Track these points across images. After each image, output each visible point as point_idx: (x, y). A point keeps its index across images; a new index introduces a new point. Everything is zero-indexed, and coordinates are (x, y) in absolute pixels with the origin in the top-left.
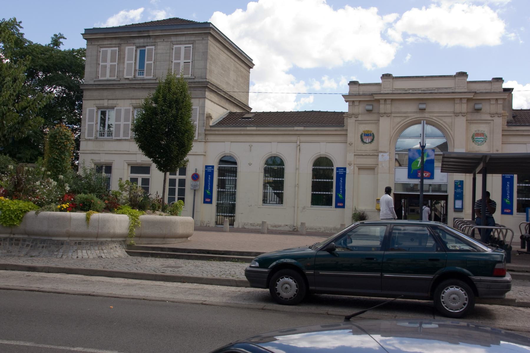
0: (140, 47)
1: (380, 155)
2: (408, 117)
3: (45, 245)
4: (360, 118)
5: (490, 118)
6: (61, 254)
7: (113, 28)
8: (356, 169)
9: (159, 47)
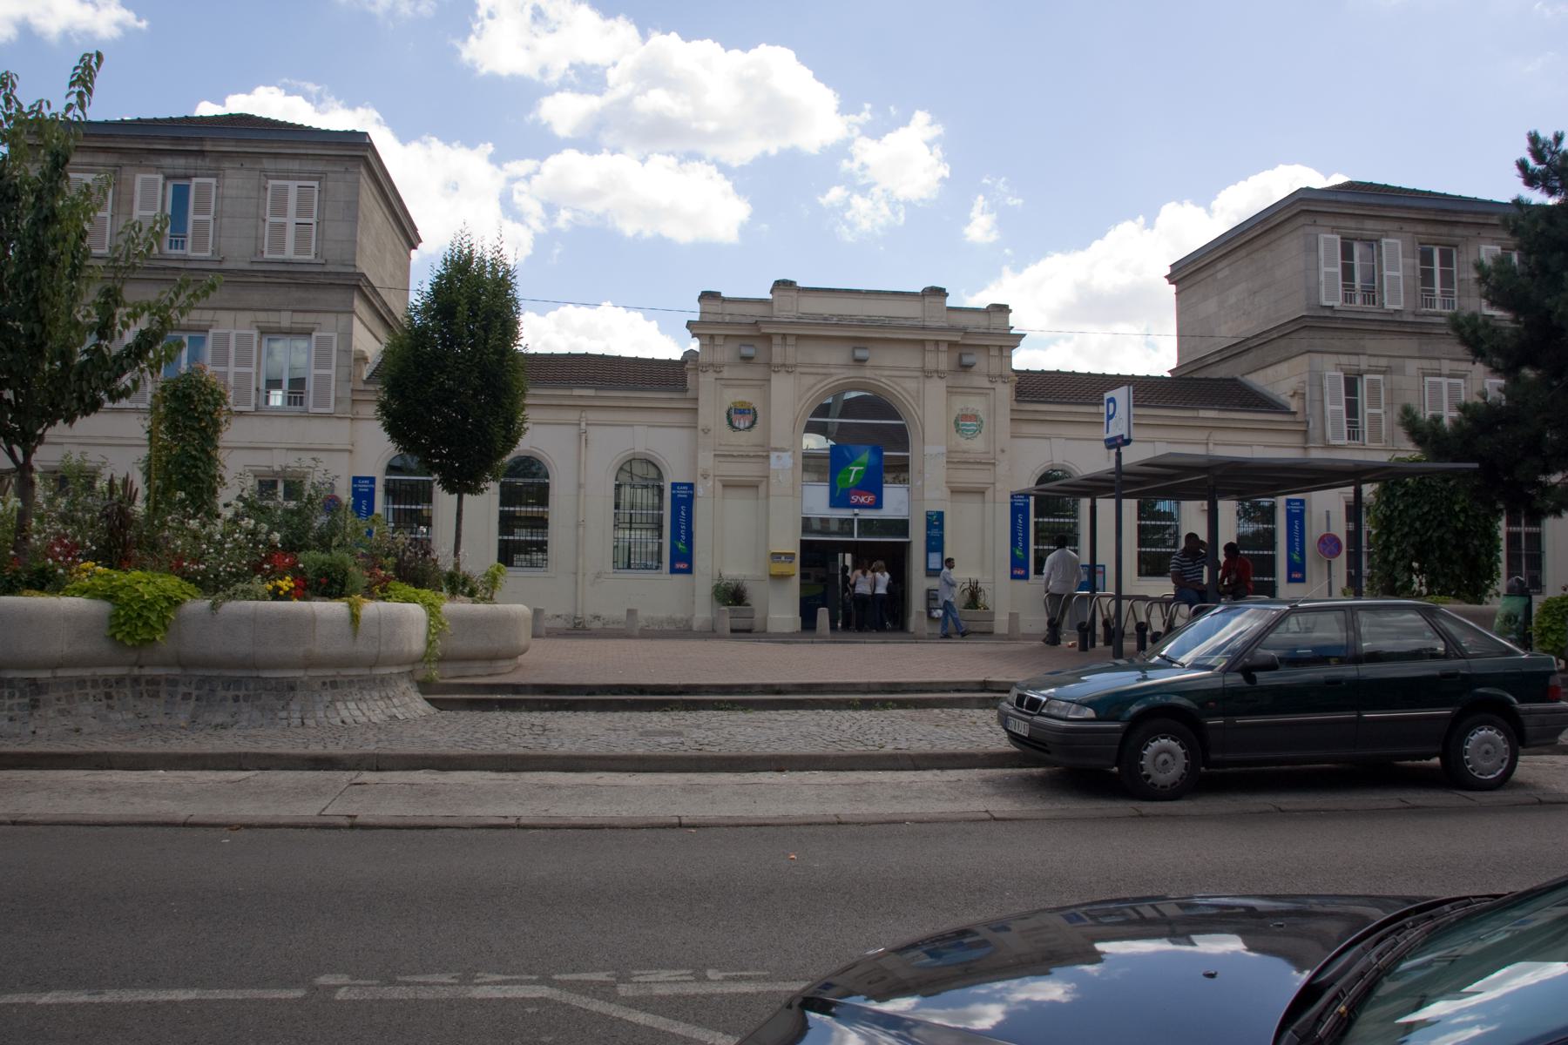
0: (175, 177)
1: (773, 455)
2: (831, 375)
3: (241, 693)
4: (726, 373)
5: (989, 385)
6: (298, 715)
7: (106, 123)
8: (719, 486)
9: (227, 181)
